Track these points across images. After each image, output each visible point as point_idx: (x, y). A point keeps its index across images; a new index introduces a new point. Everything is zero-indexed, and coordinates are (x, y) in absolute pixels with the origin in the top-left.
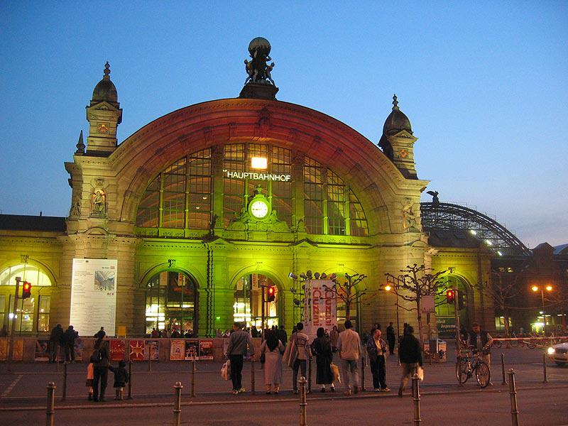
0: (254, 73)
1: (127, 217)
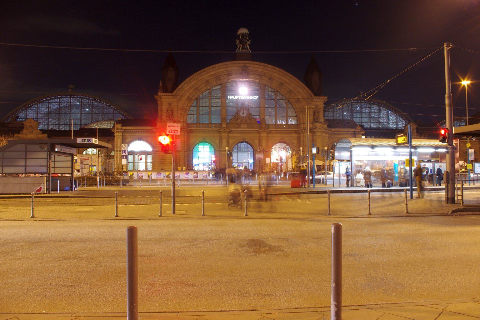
0: (240, 46)
1: (183, 119)
